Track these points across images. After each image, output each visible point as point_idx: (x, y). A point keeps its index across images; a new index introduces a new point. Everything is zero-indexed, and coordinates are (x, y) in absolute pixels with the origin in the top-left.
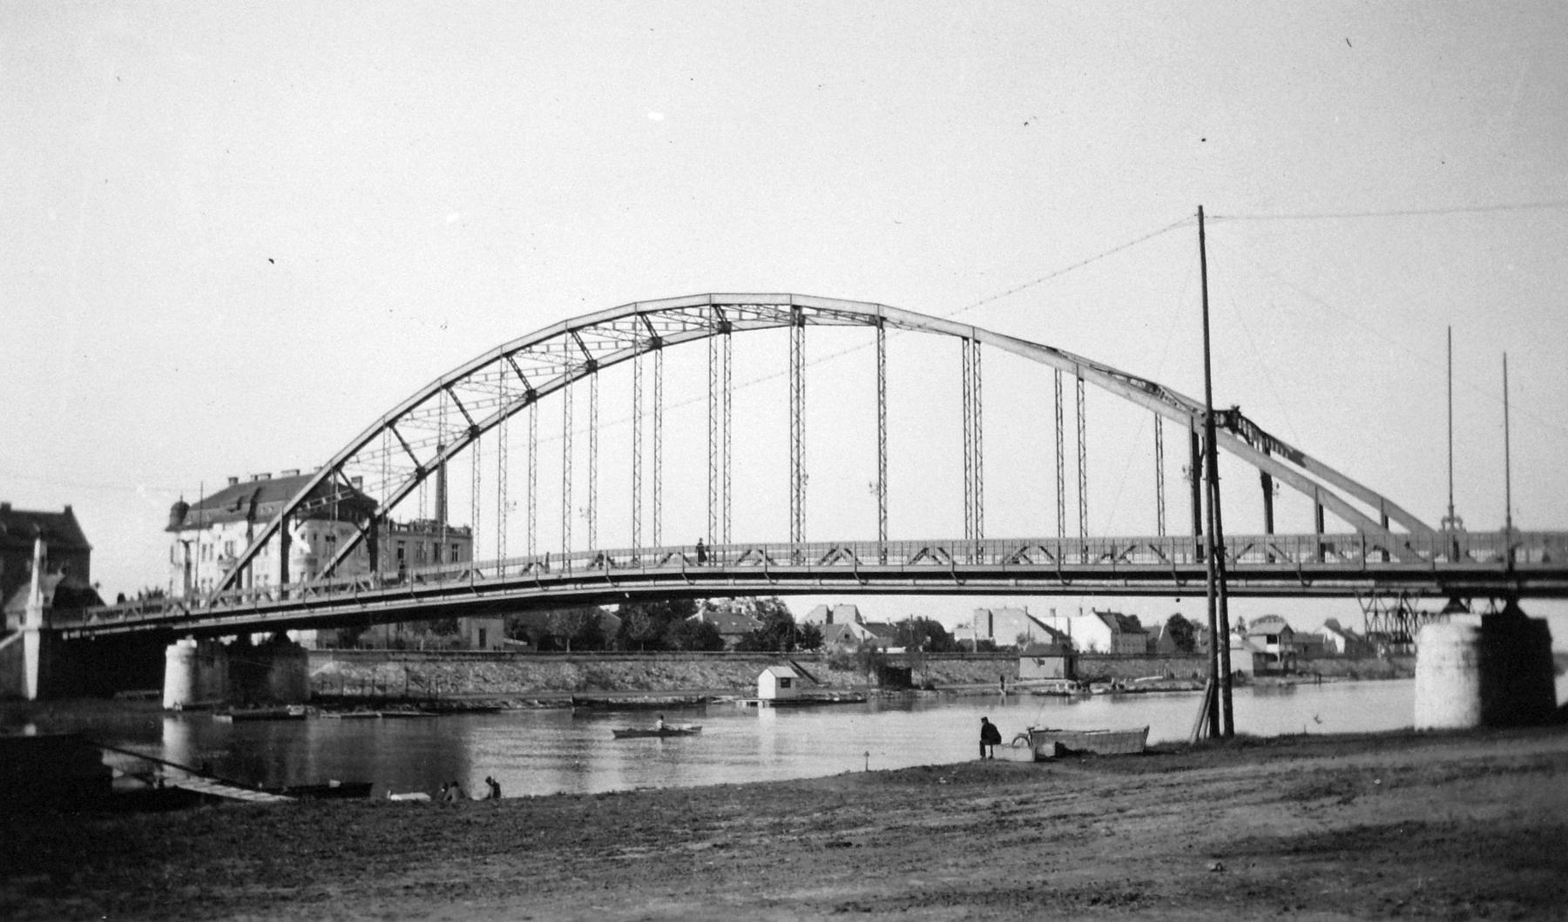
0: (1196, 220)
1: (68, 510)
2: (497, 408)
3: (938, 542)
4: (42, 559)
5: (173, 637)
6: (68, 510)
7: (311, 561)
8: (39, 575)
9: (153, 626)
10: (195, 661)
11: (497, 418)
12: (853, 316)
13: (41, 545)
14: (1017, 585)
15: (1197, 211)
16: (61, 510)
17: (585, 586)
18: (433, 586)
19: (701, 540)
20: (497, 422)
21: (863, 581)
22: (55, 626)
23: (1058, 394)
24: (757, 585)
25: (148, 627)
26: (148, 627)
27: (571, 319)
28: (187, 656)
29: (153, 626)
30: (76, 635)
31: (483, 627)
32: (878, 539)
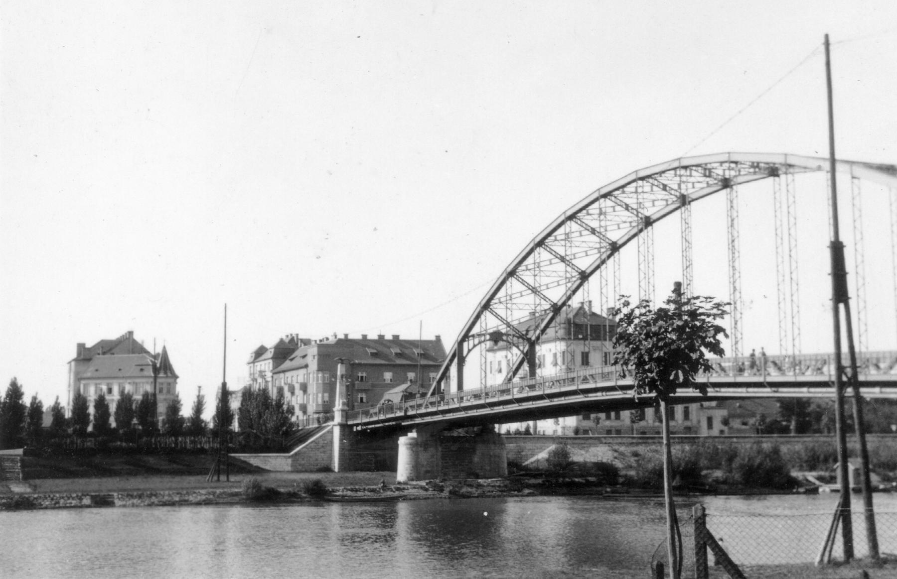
0: (822, 49)
1: (438, 338)
2: (598, 255)
3: (814, 355)
4: (342, 376)
5: (405, 430)
6: (438, 338)
7: (445, 375)
8: (340, 386)
9: (394, 423)
10: (414, 446)
11: (598, 262)
12: (805, 168)
13: (341, 368)
14: (881, 392)
15: (823, 40)
16: (433, 338)
17: (608, 393)
18: (790, 377)
19: (754, 350)
20: (598, 267)
21: (774, 389)
22: (350, 423)
23: (559, 217)
24: (616, 395)
25: (391, 423)
26: (391, 423)
27: (602, 188)
28: (410, 444)
29: (394, 423)
30: (359, 428)
31: (709, 416)
32: (830, 349)
